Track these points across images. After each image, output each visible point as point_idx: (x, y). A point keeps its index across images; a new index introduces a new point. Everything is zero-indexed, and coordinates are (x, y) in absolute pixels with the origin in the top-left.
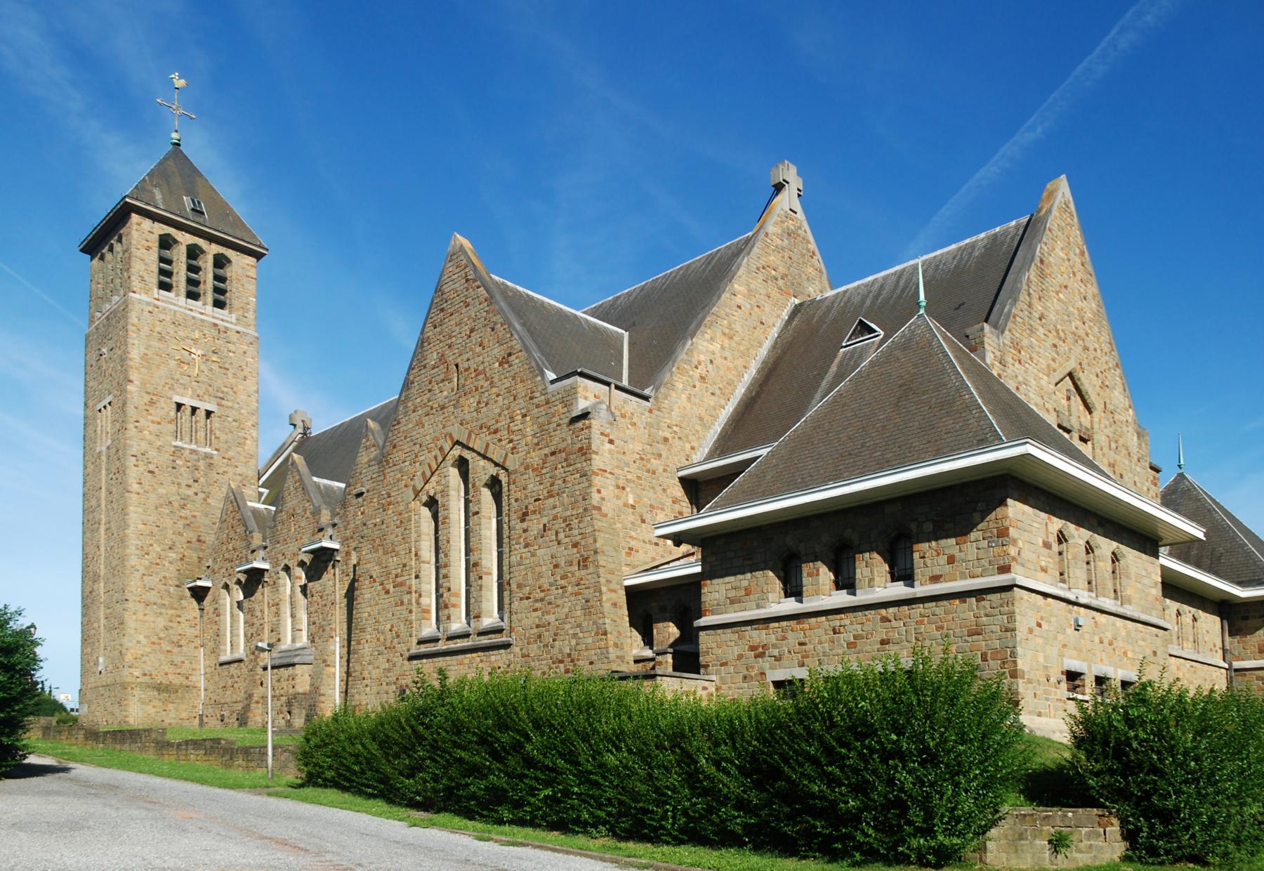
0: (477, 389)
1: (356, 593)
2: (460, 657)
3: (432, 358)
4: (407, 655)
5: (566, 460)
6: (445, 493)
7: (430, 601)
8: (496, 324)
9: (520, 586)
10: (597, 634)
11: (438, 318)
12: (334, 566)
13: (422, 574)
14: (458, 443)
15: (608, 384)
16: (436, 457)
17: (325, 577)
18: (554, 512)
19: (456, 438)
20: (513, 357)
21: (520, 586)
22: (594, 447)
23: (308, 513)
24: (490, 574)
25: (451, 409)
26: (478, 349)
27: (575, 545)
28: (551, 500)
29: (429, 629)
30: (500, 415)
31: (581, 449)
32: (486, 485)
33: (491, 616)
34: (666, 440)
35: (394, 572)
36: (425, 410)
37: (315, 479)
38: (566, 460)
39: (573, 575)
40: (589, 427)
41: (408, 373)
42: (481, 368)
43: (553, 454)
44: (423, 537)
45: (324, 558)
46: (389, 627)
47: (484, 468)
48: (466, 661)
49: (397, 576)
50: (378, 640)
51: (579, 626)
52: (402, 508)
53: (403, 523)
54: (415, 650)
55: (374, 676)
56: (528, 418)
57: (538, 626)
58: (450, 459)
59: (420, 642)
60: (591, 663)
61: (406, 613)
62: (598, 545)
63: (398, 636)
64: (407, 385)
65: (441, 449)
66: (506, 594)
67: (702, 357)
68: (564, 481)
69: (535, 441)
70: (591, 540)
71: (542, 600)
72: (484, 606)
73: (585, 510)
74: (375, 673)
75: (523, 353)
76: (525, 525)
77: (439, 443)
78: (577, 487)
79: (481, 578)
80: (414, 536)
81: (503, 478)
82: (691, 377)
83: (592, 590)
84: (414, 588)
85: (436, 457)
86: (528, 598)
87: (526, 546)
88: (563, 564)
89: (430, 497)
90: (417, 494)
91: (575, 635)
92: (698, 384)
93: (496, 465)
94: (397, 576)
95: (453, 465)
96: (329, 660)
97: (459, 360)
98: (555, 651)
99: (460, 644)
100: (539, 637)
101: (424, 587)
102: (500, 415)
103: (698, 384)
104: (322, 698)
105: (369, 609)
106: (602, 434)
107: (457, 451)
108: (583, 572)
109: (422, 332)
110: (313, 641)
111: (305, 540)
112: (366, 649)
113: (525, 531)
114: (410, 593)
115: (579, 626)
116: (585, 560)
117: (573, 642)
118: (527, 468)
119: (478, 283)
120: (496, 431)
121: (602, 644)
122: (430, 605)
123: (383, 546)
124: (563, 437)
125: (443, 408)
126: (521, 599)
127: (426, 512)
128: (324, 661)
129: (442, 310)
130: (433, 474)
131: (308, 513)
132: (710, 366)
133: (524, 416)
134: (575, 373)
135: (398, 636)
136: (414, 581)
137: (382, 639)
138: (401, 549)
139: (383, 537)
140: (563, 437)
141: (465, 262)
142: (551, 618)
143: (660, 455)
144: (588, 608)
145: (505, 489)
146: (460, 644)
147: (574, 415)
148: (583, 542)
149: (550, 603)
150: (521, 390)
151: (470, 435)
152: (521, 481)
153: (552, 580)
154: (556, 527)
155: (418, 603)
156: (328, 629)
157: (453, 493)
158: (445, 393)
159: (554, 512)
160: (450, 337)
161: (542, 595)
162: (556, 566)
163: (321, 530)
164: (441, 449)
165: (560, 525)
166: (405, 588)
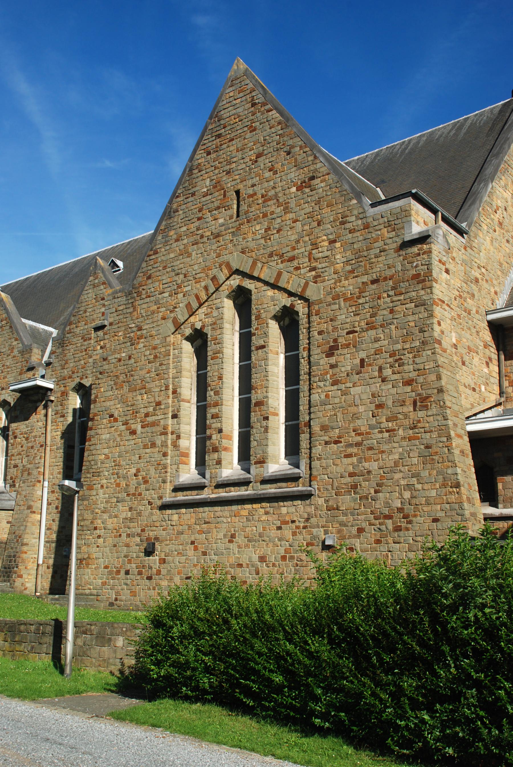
0: (265, 215)
1: (89, 433)
2: (234, 508)
3: (204, 184)
4: (159, 503)
5: (393, 288)
6: (217, 324)
7: (190, 443)
8: (292, 147)
9: (324, 428)
10: (444, 485)
11: (212, 145)
12: (46, 407)
13: (182, 413)
14: (237, 272)
15: (434, 211)
16: (206, 288)
17: (34, 418)
18: (376, 345)
19: (235, 266)
20: (317, 181)
21: (324, 428)
22: (434, 274)
23: (16, 352)
24: (277, 415)
25: (229, 237)
26: (267, 174)
27: (408, 383)
28: (372, 333)
29: (189, 474)
30: (298, 242)
31: (416, 276)
32: (275, 317)
33: (277, 462)
34: (477, 280)
35: (143, 411)
36: (192, 239)
37: (24, 320)
38: (393, 288)
39: (406, 416)
40: (430, 252)
41: (171, 202)
42: (272, 193)
43: (373, 282)
44: (184, 373)
45: (35, 398)
46: (133, 471)
47: (273, 299)
48: (245, 513)
49: (147, 415)
50: (118, 485)
51: (416, 475)
52: (157, 342)
53: (159, 357)
54: (169, 497)
55: (110, 526)
56: (338, 245)
57: (351, 475)
58: (225, 290)
59: (177, 489)
60: (436, 520)
61: (158, 457)
62: (443, 382)
63: (146, 482)
64: (168, 213)
65: (214, 279)
66: (304, 438)
67: (499, 203)
68: (392, 311)
69: (349, 268)
70: (433, 377)
71: (358, 444)
72: (271, 450)
73: (423, 343)
74: (111, 523)
75: (332, 176)
76: (332, 360)
77: (215, 271)
78: (411, 318)
79: (267, 418)
80: (172, 372)
81: (300, 307)
82: (492, 220)
83: (435, 435)
84: (170, 429)
85: (206, 288)
86: (336, 442)
87: (335, 383)
88: (390, 403)
89: (196, 330)
90: (178, 326)
91: (409, 487)
92: (497, 229)
93: (291, 294)
94: (147, 415)
95: (228, 297)
96: (36, 506)
97: (240, 187)
98: (379, 505)
99: (235, 493)
100: (354, 487)
101: (184, 428)
102: (298, 242)
103: (497, 229)
104: (25, 548)
105: (106, 451)
106: (440, 261)
107: (235, 281)
108: (421, 414)
109: (191, 159)
110: (13, 485)
111: (10, 378)
112: (100, 493)
113: (332, 366)
114: (166, 434)
115: (416, 475)
116: (424, 399)
117: (407, 495)
118: (336, 297)
119: (269, 106)
120: (292, 259)
121: (453, 498)
122: (188, 449)
123: (128, 381)
124: (389, 263)
125: (217, 236)
126: (326, 443)
127: (187, 347)
128: (30, 507)
129: (219, 136)
130: (201, 305)
131: (16, 352)
132: (505, 213)
133: (332, 242)
134: (409, 194)
135: (146, 482)
136: (170, 421)
137: (123, 483)
138: (155, 386)
139: (129, 373)
140: (389, 263)
141: (251, 85)
142: (373, 466)
143: (473, 295)
144: (428, 454)
145: (303, 320)
146: (235, 493)
147: (407, 238)
148: (421, 379)
149: (371, 448)
150: (328, 214)
151: (254, 264)
152: (327, 312)
153: (373, 421)
154: (380, 362)
155: (175, 446)
156: (35, 472)
157: (227, 326)
158: (221, 221)
159: (376, 345)
160: (229, 163)
161: (359, 439)
162: (380, 406)
163: (31, 369)
164: (214, 279)
165: (384, 359)
166: (159, 429)
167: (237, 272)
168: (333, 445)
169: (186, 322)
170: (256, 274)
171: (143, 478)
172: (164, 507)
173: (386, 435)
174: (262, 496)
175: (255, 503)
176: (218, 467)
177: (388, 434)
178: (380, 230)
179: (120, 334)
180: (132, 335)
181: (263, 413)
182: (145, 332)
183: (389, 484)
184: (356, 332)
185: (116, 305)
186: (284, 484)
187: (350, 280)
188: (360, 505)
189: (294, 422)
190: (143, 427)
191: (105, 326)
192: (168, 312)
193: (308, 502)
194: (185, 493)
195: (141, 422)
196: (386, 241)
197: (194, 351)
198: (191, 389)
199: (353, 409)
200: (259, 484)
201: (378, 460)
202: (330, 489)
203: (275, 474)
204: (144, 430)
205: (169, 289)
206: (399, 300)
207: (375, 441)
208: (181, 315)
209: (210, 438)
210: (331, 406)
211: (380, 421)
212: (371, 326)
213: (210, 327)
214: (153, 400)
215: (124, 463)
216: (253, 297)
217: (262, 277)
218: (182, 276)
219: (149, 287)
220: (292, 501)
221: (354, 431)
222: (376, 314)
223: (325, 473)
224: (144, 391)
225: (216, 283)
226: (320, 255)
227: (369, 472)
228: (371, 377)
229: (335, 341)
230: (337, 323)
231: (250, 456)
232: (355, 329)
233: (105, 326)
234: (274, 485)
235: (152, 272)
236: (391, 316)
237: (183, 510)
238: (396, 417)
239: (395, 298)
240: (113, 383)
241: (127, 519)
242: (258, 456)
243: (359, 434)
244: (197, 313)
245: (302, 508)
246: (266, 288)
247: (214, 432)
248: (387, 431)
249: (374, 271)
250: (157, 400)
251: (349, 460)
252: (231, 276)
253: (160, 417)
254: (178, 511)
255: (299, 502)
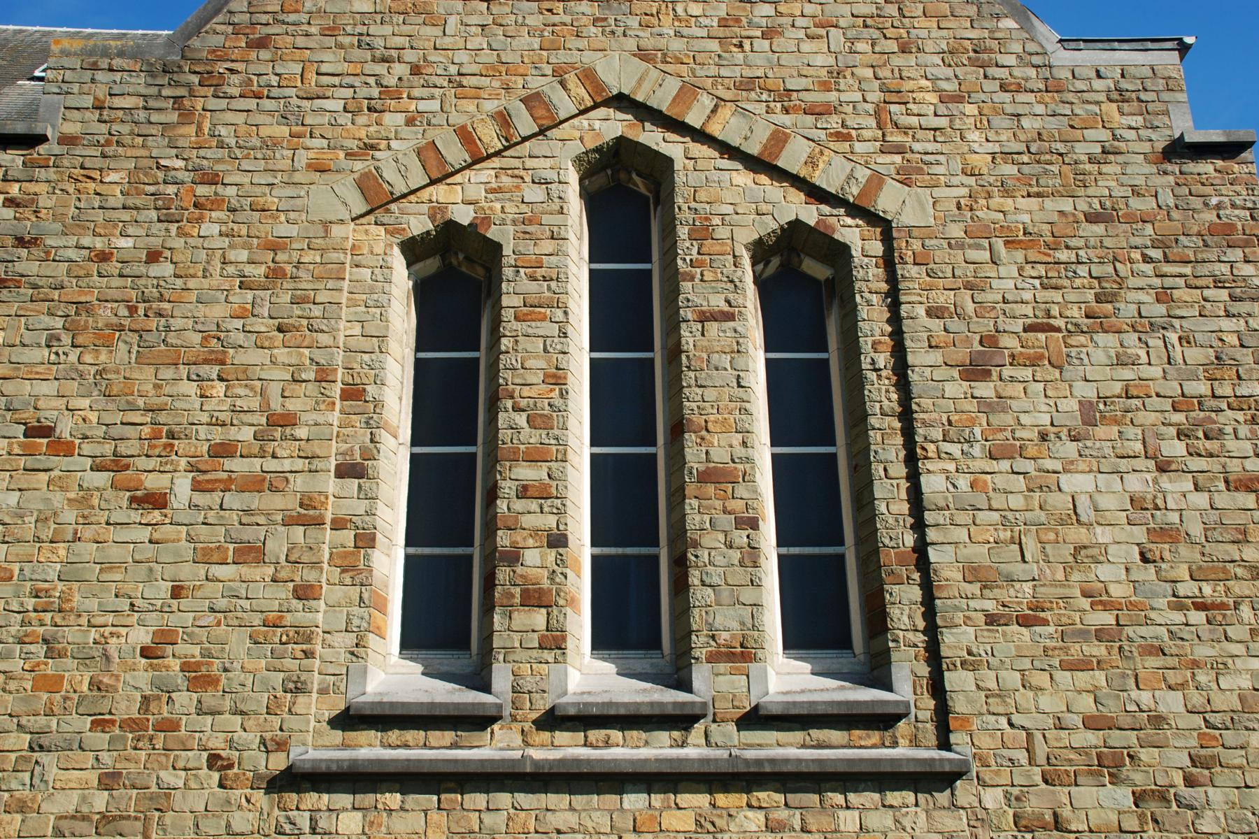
2: (634, 801)
14: (622, 102)
43: (1092, 218)
46: (142, 636)
49: (223, 450)
54: (318, 746)
86: (1024, 622)
90: (378, 201)
113: (987, 407)
130: (478, 160)
136: (331, 484)
138: (272, 364)
146: (624, 749)
161: (1108, 618)
166: (285, 502)
167: (622, 102)
168: (1015, 628)
169: (412, 198)
170: (694, 119)
171: (185, 668)
172: (295, 780)
173: (1197, 617)
174: (768, 769)
175: (726, 790)
176: (548, 656)
177: (1203, 614)
178: (1098, 103)
179: (113, 177)
180: (171, 189)
181: (737, 505)
182: (231, 191)
183: (1237, 762)
184: (1058, 330)
185: (101, 92)
186: (835, 736)
187: (1020, 200)
188: (1141, 818)
189: (459, 551)
190: (197, 487)
191: (43, 139)
192: (342, 155)
193: (943, 797)
194: (394, 736)
195: (193, 468)
196: (1117, 132)
197: (415, 287)
198: (400, 399)
199: (1077, 534)
200: (732, 727)
201: (1182, 686)
202: (1024, 761)
203: (789, 698)
204: (200, 499)
205: (348, 93)
206: (1181, 276)
207: (1164, 629)
208: (399, 167)
209: (514, 558)
210: (996, 516)
211: (1172, 575)
212: (1097, 322)
213: (511, 228)
214: (255, 403)
215: (93, 604)
216: (680, 178)
217: (715, 129)
218: (400, 69)
219: (253, 68)
220: (881, 790)
221: (1085, 594)
222: (1115, 295)
223: (1001, 710)
224: (214, 371)
225: (541, 112)
226: (914, 121)
227: (1158, 721)
228: (1119, 452)
229: (989, 341)
230: (989, 297)
231: (690, 632)
232: (1052, 321)
233: (43, 139)
234: (798, 736)
235: (269, 30)
236: (1161, 309)
237: (393, 799)
238: (1224, 570)
239: (1168, 269)
240: (59, 323)
241: (85, 818)
242: (725, 635)
243: (1107, 606)
244: (458, 178)
245: (923, 816)
246: (725, 163)
247: (531, 542)
248: (1200, 607)
249: (1090, 191)
250: (276, 405)
251: (1083, 678)
252: (596, 106)
253: (287, 465)
254: (368, 799)
255: (909, 797)
